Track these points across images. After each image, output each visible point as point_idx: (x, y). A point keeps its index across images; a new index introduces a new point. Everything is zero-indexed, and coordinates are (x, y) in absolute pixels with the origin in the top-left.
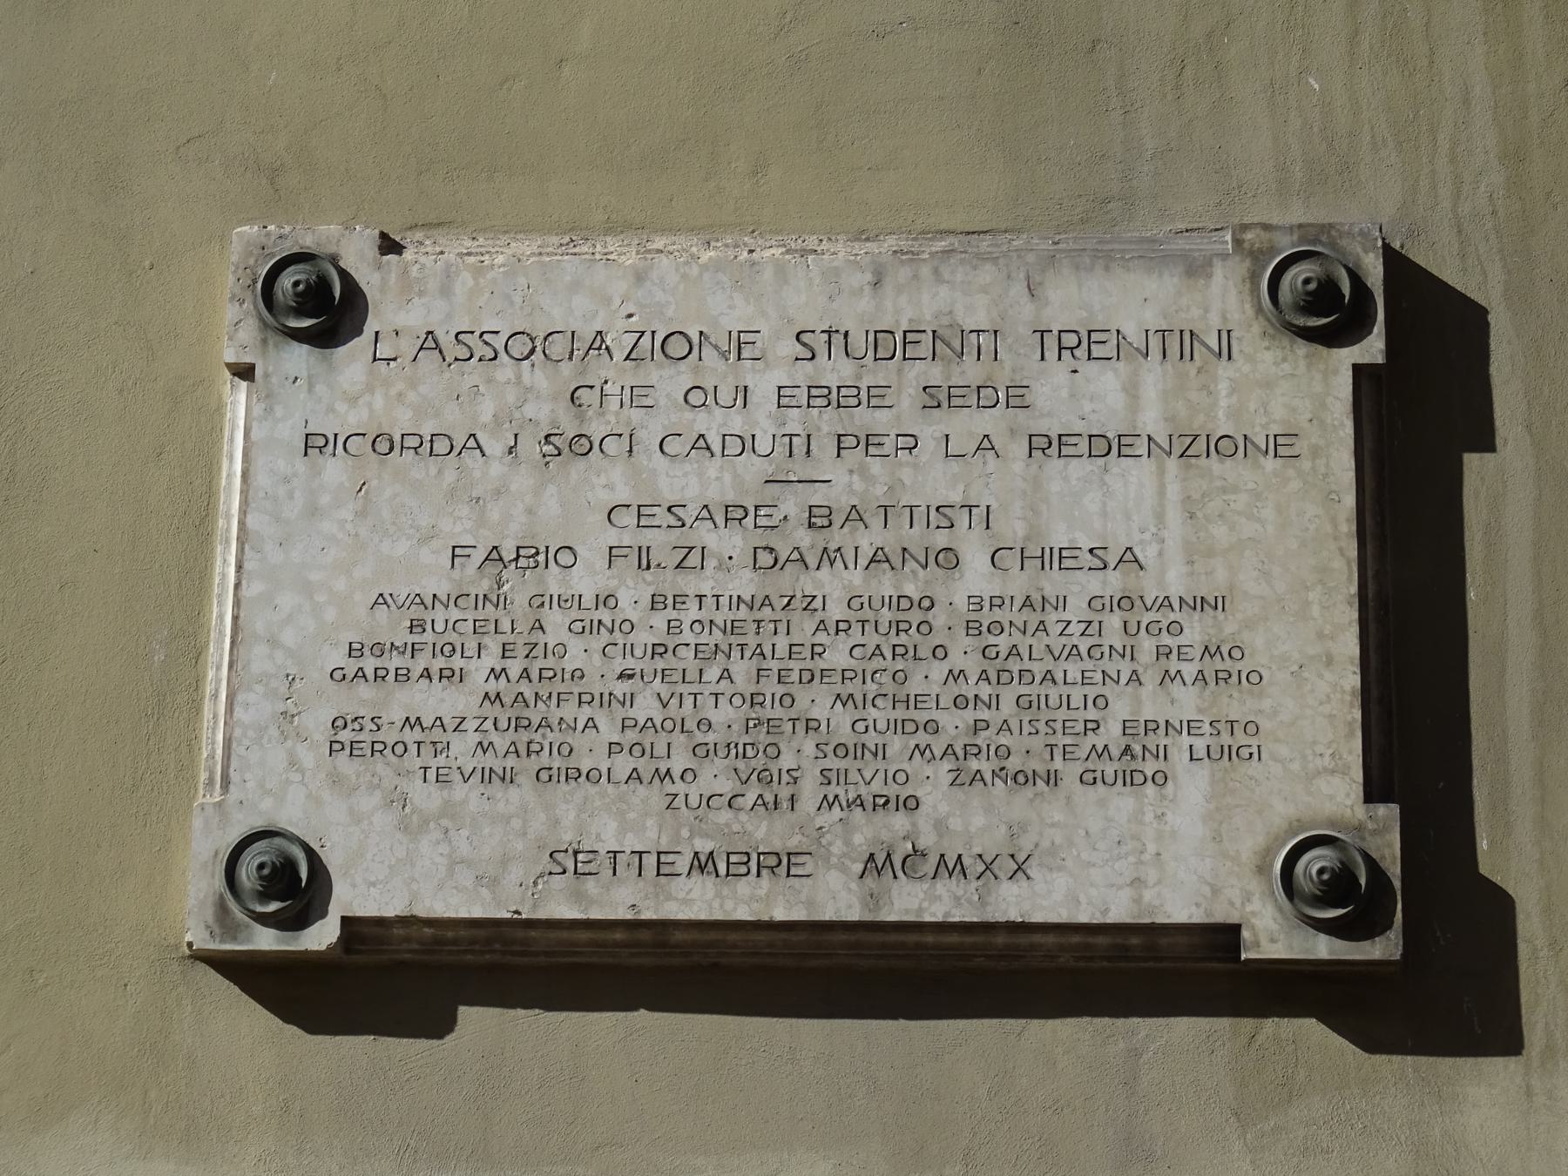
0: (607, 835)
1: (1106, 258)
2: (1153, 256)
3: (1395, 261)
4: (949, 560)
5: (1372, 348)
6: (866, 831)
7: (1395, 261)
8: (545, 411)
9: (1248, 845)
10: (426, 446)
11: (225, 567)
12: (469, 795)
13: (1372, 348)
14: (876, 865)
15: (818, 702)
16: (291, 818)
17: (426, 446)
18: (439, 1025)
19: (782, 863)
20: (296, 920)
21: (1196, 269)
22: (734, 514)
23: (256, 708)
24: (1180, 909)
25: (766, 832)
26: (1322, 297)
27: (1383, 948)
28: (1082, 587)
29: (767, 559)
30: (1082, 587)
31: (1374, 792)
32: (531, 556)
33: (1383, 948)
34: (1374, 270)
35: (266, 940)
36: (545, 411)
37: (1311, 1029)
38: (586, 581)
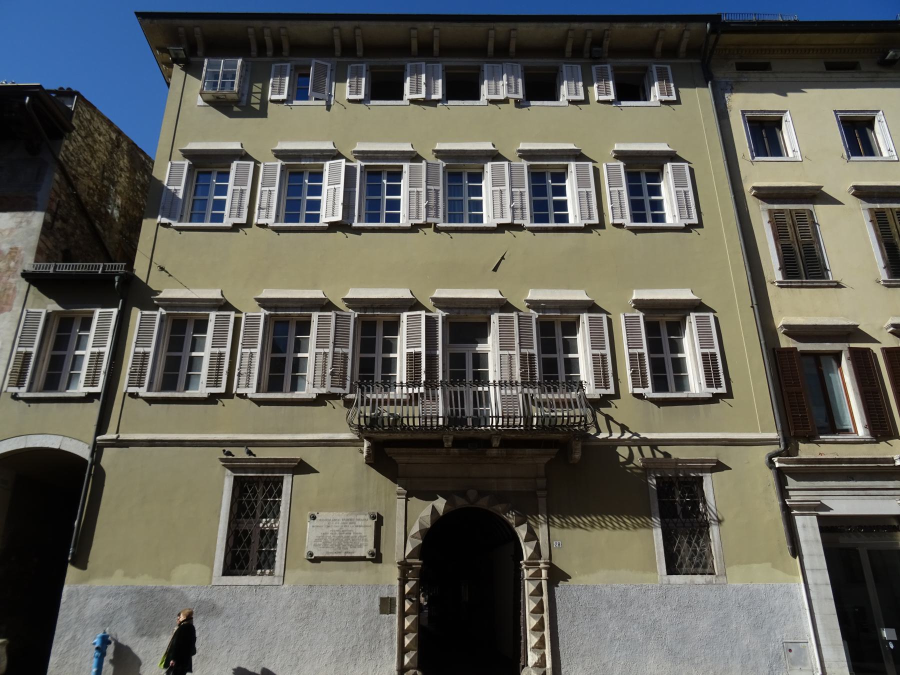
0: (330, 551)
1: (360, 514)
2: (363, 514)
3: (378, 514)
4: (350, 534)
5: (376, 520)
6: (345, 551)
7: (378, 514)
8: (327, 524)
9: (367, 551)
10: (320, 526)
11: (308, 534)
12: (322, 549)
13: (376, 520)
14: (345, 553)
15: (343, 543)
16: (311, 550)
17: (320, 526)
18: (320, 562)
19: (340, 553)
20: (311, 557)
21: (366, 515)
22: (338, 531)
23: (309, 543)
24: (363, 555)
25: (339, 551)
26: (373, 517)
27: (374, 557)
28: (359, 535)
29: (340, 534)
30: (359, 535)
31: (374, 548)
32: (326, 533)
33: (374, 557)
34: (376, 515)
35: (310, 558)
36: (327, 524)
37: (370, 562)
38: (329, 535)
